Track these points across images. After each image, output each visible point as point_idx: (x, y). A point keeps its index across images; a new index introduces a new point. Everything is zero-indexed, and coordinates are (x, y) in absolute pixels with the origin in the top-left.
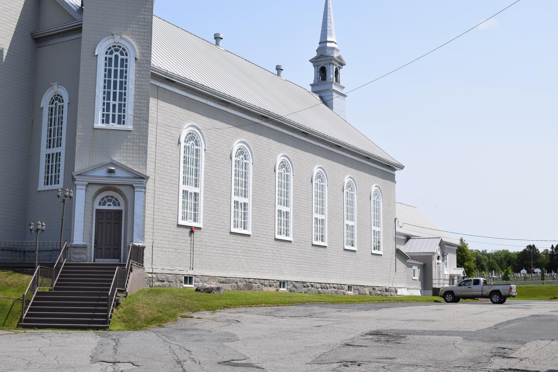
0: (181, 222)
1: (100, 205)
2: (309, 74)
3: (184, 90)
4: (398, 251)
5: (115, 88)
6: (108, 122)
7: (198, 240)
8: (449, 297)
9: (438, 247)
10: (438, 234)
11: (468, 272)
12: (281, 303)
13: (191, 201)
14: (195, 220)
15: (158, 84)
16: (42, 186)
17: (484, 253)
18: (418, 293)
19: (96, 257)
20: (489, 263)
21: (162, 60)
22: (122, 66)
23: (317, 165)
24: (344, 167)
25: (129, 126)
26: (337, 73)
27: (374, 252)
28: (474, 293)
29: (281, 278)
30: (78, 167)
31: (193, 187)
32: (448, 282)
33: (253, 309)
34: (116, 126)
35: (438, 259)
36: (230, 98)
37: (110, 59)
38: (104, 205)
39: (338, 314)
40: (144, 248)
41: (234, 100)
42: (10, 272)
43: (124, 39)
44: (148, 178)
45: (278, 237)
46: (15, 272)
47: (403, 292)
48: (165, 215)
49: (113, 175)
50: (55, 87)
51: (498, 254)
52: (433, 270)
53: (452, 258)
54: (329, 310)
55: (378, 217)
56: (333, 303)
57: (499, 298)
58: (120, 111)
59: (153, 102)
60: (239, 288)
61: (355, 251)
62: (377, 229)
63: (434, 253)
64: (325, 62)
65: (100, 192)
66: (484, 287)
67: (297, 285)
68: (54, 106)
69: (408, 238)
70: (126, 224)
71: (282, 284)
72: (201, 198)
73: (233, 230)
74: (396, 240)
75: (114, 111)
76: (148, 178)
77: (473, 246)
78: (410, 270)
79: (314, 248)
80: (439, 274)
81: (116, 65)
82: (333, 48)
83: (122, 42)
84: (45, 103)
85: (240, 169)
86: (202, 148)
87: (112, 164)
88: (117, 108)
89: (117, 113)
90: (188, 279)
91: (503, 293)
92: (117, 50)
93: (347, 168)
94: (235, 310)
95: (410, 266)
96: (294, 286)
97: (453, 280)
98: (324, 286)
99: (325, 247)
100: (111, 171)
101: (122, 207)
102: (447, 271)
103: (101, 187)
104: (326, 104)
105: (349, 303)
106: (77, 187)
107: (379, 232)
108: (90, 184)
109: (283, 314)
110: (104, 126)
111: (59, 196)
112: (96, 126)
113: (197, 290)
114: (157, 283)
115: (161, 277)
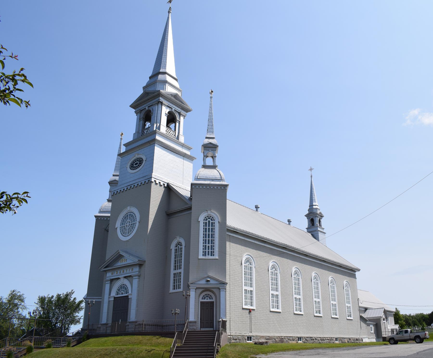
0: (244, 307)
1: (202, 299)
2: (305, 223)
3: (243, 236)
4: (361, 317)
5: (209, 237)
6: (205, 255)
7: (254, 316)
8: (392, 341)
9: (383, 314)
10: (382, 306)
11: (401, 327)
12: (301, 349)
13: (249, 295)
14: (251, 305)
15: (230, 234)
16: (171, 291)
17: (410, 316)
18: (374, 340)
19: (201, 327)
20: (413, 321)
21: (232, 221)
22: (212, 226)
23: (314, 272)
24: (328, 272)
25: (216, 257)
26: (320, 221)
27: (348, 318)
28: (405, 338)
29: (299, 336)
30: (191, 279)
31: (250, 287)
32: (390, 333)
33: (287, 352)
34: (210, 257)
35: (384, 320)
36: (267, 239)
37: (206, 223)
38: (204, 299)
39: (333, 353)
40: (226, 321)
41: (269, 240)
42: (157, 337)
43: (213, 212)
44: (227, 283)
45: (296, 312)
46: (163, 337)
47: (366, 340)
48: (236, 303)
49: (209, 283)
50: (178, 238)
51: (417, 315)
52: (382, 327)
53: (391, 319)
54: (327, 351)
55: (348, 298)
56: (328, 348)
57: (420, 340)
58: (211, 249)
59: (228, 243)
60: (276, 342)
61: (337, 318)
62: (349, 305)
63: (381, 317)
64: (313, 216)
65: (201, 293)
66: (411, 334)
67: (308, 339)
68: (177, 248)
69: (366, 309)
70: (216, 309)
71: (300, 339)
72: (254, 293)
73: (272, 310)
74: (360, 311)
75: (208, 249)
76: (227, 283)
77: (403, 312)
78: (369, 327)
79: (315, 318)
80: (385, 328)
81: (209, 226)
82: (317, 209)
83: (212, 214)
84: (173, 247)
85: (274, 276)
86: (253, 266)
87: (209, 277)
88: (210, 247)
89: (210, 250)
90: (249, 338)
91: (421, 337)
92: (209, 218)
93: (330, 272)
94: (277, 353)
95: (368, 325)
96: (306, 340)
97: (393, 332)
98: (322, 339)
99: (321, 317)
100: (208, 281)
101: (214, 300)
102: (390, 327)
103: (203, 289)
104: (315, 238)
105: (337, 347)
106: (191, 290)
107: (350, 307)
108: (197, 288)
109: (303, 354)
110: (204, 257)
111: (183, 295)
112: (199, 257)
113: (255, 343)
114: (233, 341)
115: (235, 338)
